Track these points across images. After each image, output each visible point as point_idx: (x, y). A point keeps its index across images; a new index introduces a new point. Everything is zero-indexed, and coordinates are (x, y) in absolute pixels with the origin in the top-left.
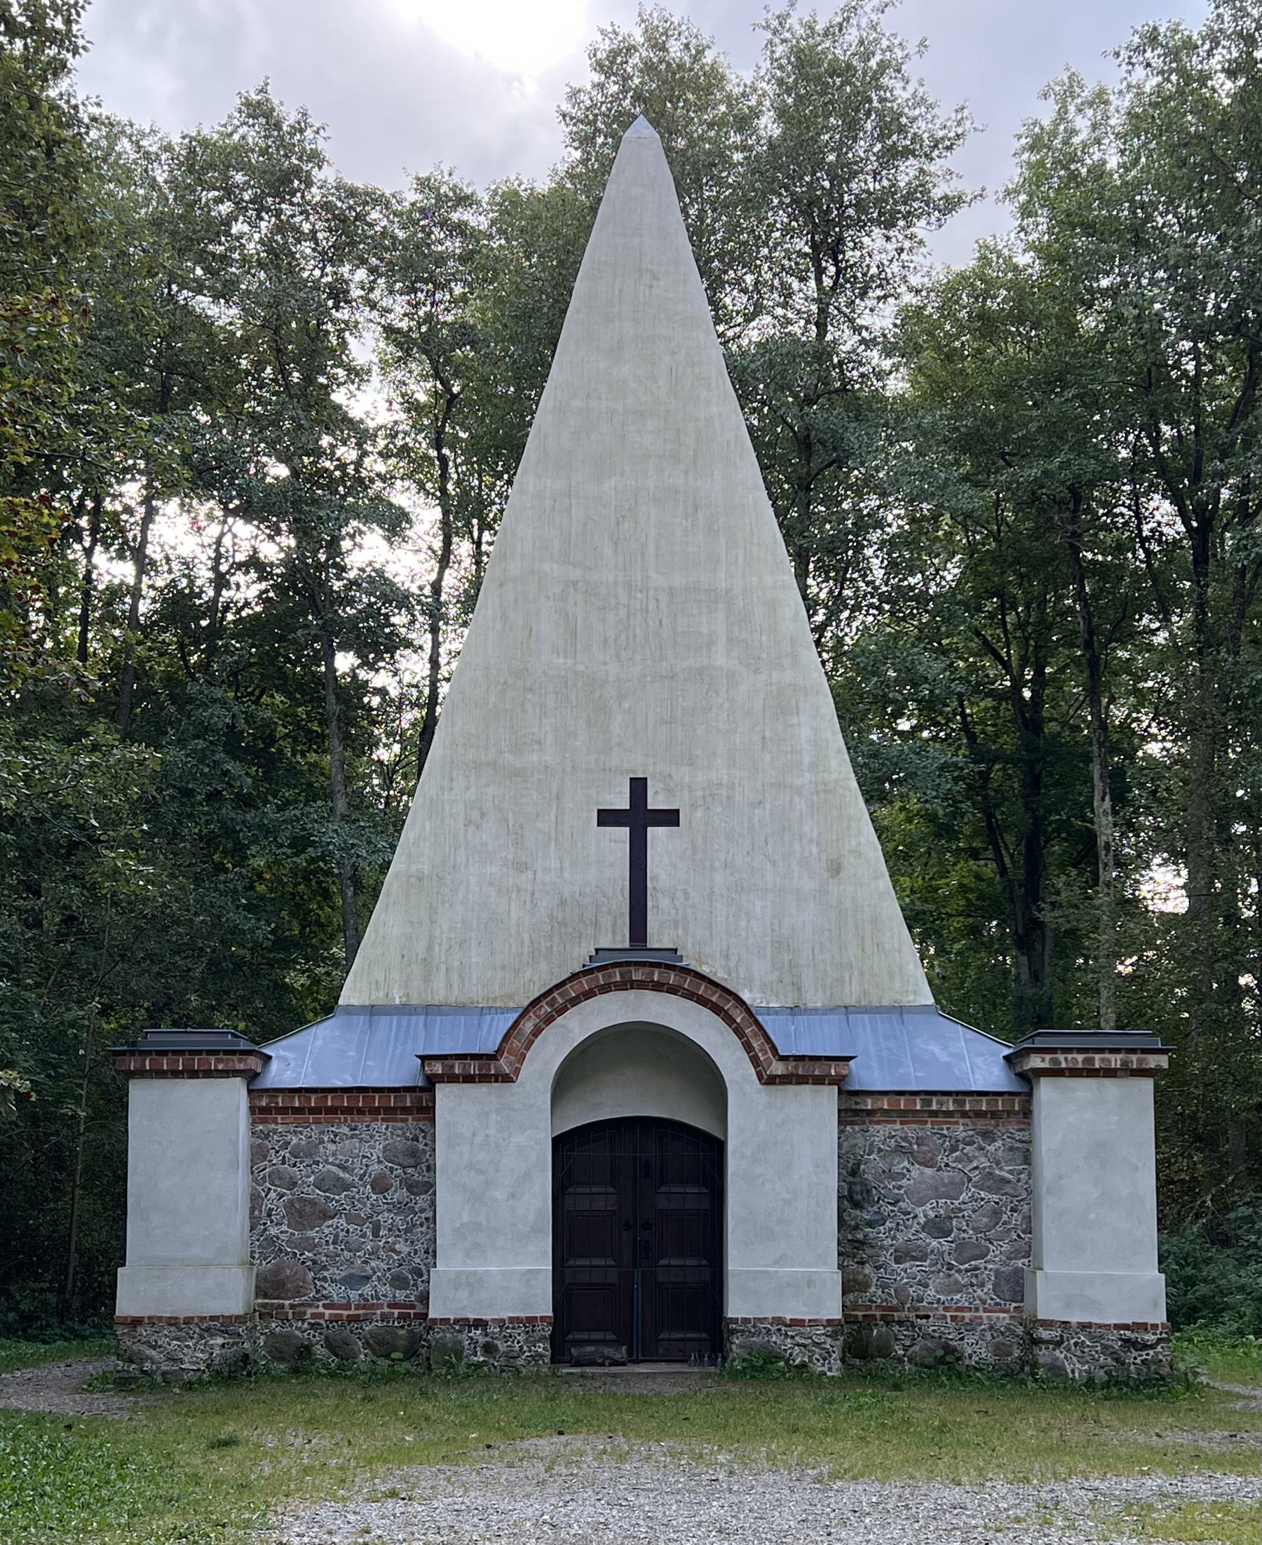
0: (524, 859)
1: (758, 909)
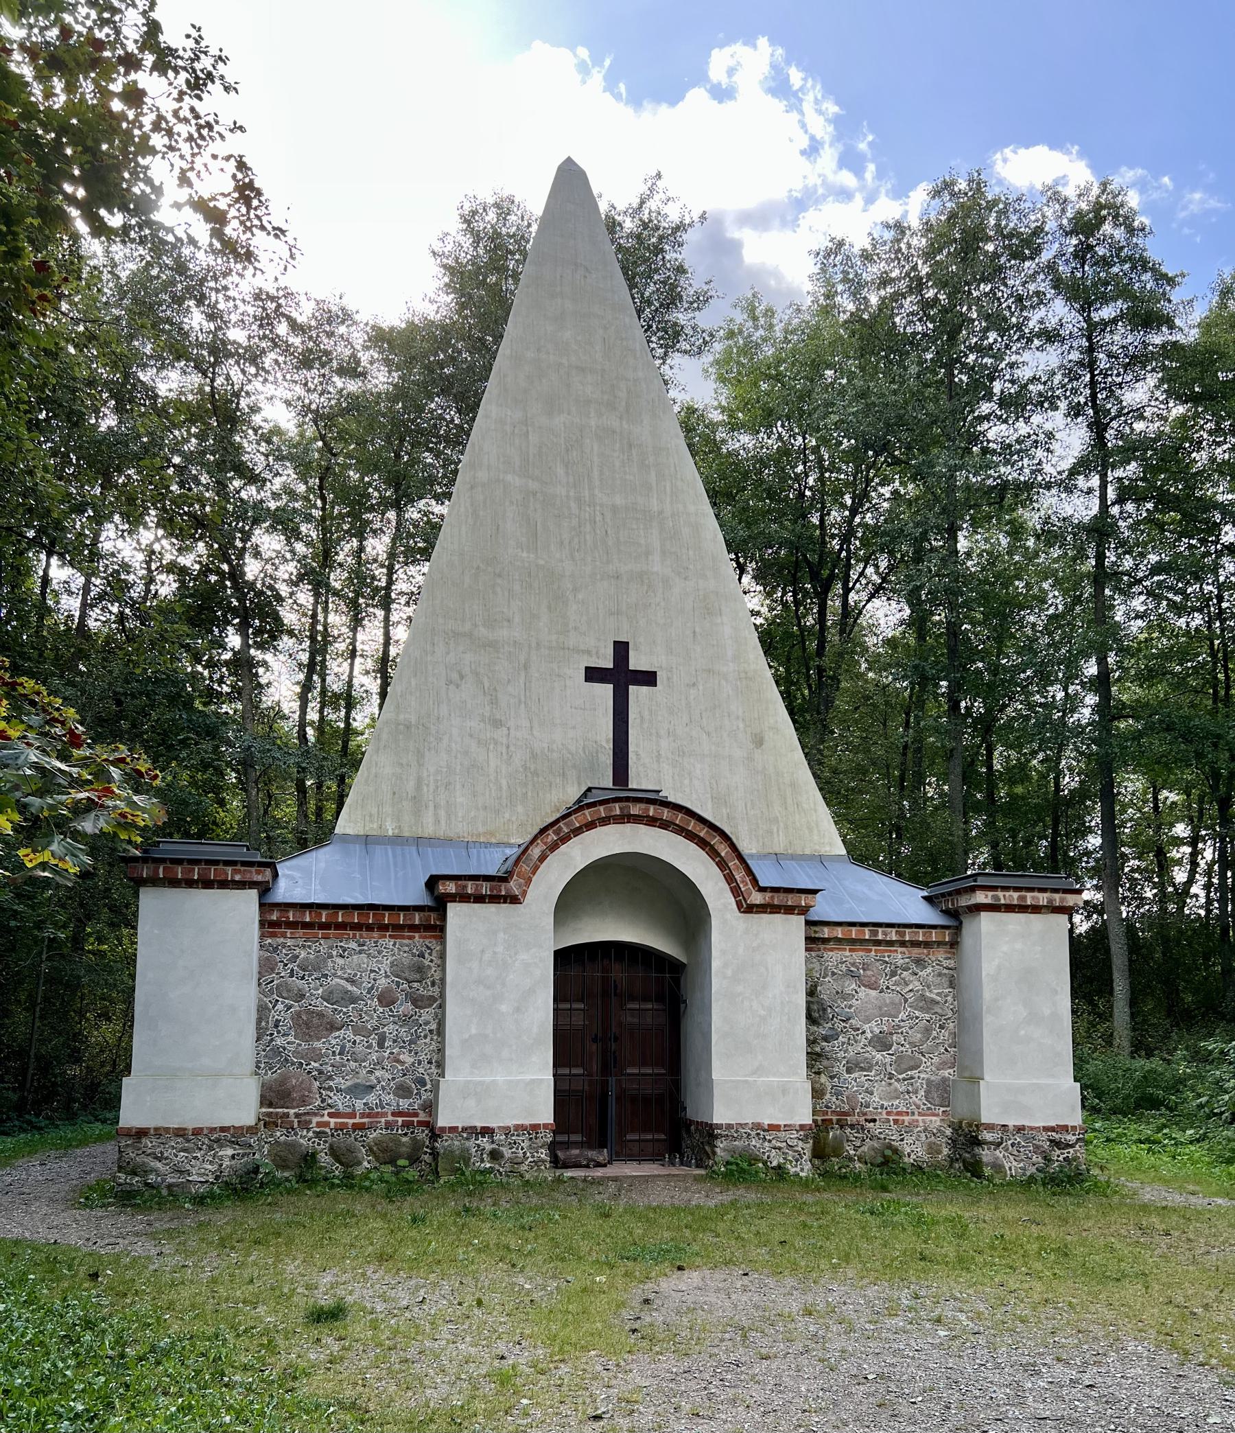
0: (498, 717)
1: (698, 771)
